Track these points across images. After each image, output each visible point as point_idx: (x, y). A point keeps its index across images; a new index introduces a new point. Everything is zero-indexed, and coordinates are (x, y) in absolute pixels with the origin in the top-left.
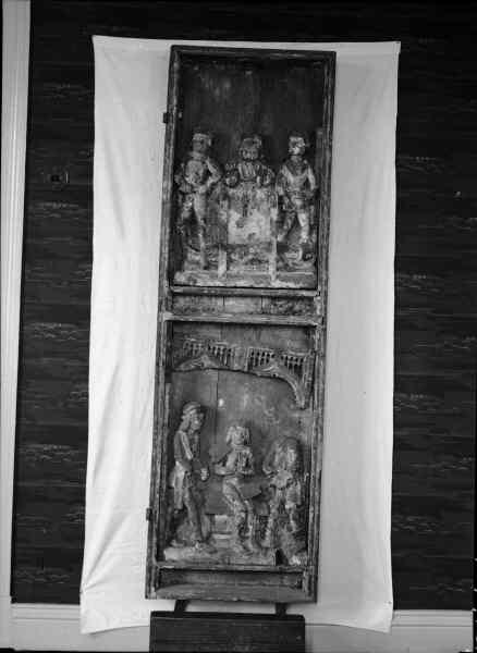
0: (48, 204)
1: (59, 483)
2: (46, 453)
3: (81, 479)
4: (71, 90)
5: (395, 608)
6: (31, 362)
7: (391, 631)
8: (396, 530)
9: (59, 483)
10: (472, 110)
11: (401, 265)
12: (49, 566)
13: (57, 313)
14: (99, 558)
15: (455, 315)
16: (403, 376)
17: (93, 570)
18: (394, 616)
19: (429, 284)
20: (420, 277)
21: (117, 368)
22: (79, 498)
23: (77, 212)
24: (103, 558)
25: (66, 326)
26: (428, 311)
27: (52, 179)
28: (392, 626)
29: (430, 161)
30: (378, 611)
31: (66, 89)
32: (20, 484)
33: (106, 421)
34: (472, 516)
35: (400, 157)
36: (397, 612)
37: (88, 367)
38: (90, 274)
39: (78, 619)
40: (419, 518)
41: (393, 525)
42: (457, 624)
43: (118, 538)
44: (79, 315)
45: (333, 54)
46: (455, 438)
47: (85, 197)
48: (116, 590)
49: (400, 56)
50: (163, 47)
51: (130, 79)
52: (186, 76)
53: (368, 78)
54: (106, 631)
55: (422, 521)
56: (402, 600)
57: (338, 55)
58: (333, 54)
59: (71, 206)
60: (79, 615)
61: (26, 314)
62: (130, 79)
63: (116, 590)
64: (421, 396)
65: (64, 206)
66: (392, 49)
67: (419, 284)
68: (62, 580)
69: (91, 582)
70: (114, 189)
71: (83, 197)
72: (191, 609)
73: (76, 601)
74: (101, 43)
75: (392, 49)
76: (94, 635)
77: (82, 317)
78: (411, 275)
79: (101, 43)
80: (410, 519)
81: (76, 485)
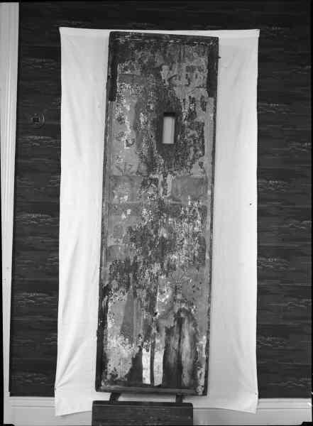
0: (31, 137)
1: (39, 317)
2: (32, 298)
3: (54, 315)
4: (44, 140)
5: (260, 397)
6: (16, 319)
7: (257, 412)
8: (260, 267)
9: (39, 317)
10: (309, 222)
11: (261, 173)
12: (37, 374)
13: (36, 208)
14: (64, 372)
15: (296, 206)
16: (263, 246)
17: (61, 376)
18: (259, 402)
19: (281, 110)
20: (275, 105)
21: (77, 243)
22: (53, 328)
23: (48, 220)
24: (66, 372)
25: (41, 294)
26: (278, 282)
27: (34, 120)
28: (257, 409)
29: (278, 184)
30: (248, 401)
31: (38, 217)
32: (16, 319)
33: (69, 283)
34: (310, 103)
35: (261, 206)
36: (262, 400)
37: (58, 242)
38: (59, 182)
39: (53, 407)
40: (274, 338)
41: (258, 343)
42: (302, 408)
43: (76, 358)
44: (51, 207)
45: (216, 40)
46: (296, 366)
47: (56, 132)
48: (76, 389)
49: (259, 38)
50: (105, 33)
51: (83, 52)
52: (117, 53)
53: (240, 48)
54: (73, 414)
55: (276, 341)
56: (264, 392)
57: (220, 43)
58: (216, 40)
59: (43, 216)
60: (54, 403)
61: (21, 131)
62: (83, 52)
63: (76, 389)
64: (276, 182)
65: (42, 137)
66: (253, 35)
67: (274, 110)
68: (43, 381)
69: (62, 382)
70: (75, 127)
71: (54, 131)
72: (121, 399)
73: (53, 395)
74: (65, 32)
75: (253, 35)
76: (64, 416)
77: (54, 210)
78: (268, 180)
79: (65, 32)
80: (268, 339)
81: (52, 320)
